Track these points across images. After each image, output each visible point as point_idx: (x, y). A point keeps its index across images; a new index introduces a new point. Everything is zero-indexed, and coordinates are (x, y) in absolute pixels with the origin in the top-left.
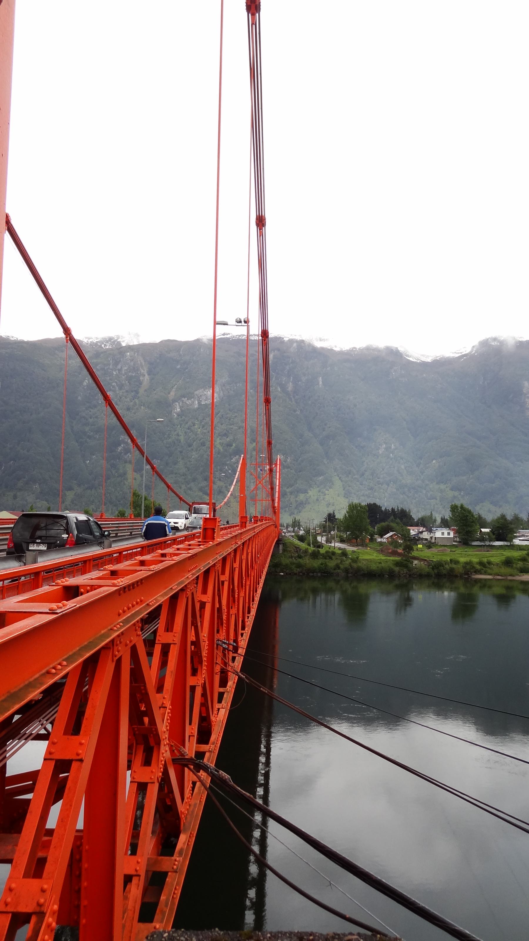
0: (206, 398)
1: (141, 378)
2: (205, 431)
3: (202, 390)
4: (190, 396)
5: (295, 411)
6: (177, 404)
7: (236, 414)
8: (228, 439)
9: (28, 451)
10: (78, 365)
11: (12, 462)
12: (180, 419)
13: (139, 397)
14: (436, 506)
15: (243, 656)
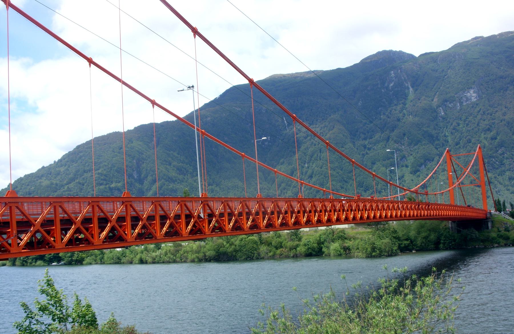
1: (406, 91)
7: (496, 109)
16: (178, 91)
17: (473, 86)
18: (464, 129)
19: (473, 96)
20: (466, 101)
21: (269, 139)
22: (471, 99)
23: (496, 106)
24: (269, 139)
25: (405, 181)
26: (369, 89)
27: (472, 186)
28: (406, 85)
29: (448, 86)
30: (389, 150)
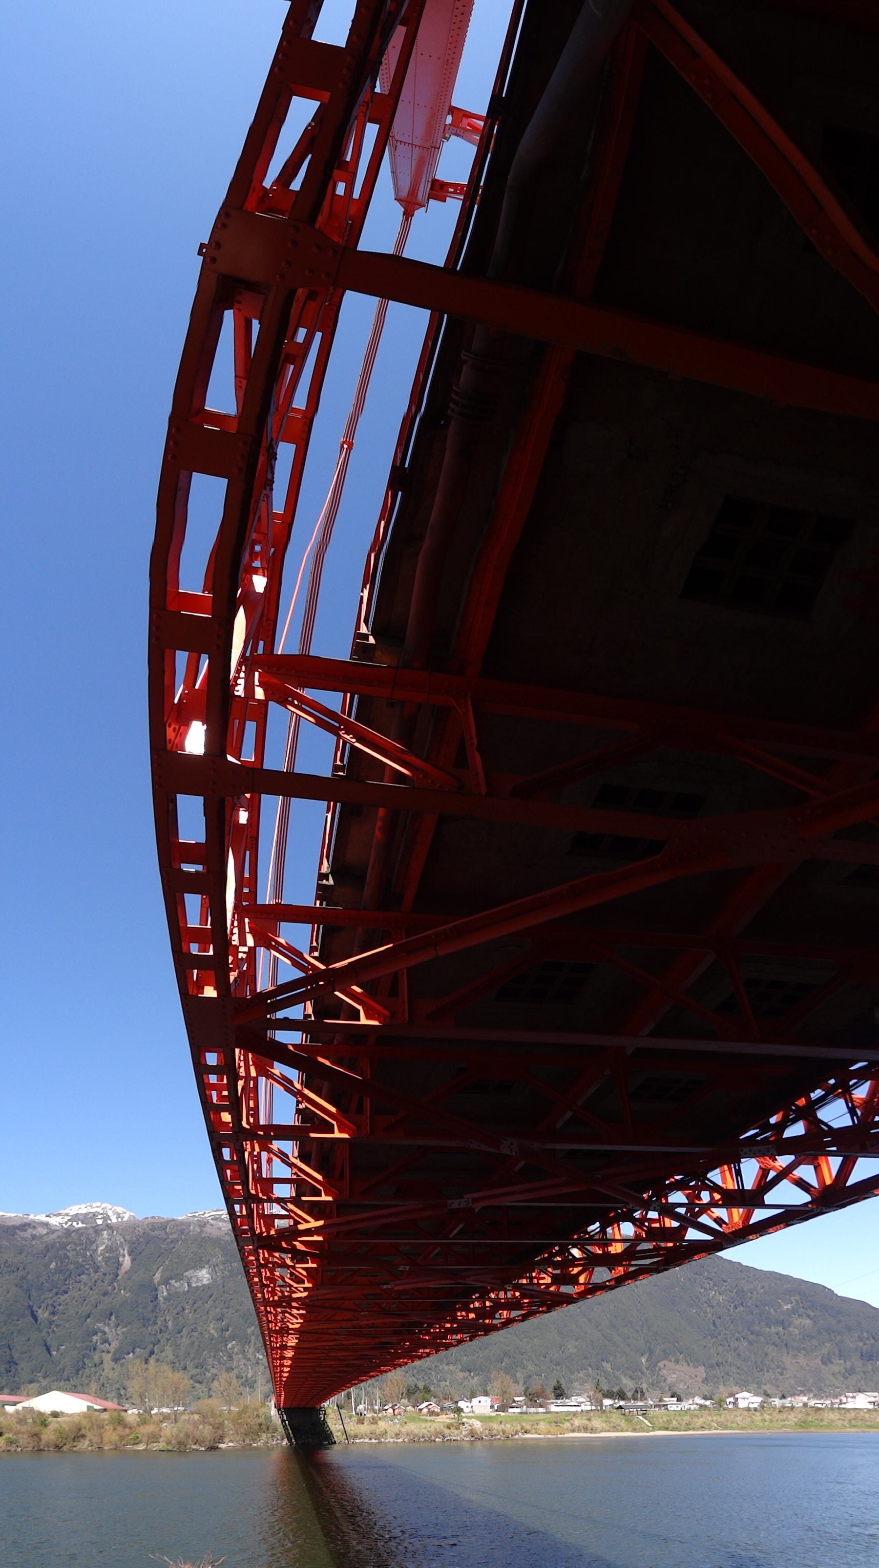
0: (198, 1280)
1: (121, 1259)
2: (196, 1316)
3: (193, 1271)
4: (179, 1277)
7: (232, 1297)
12: (168, 1303)
13: (118, 1281)
14: (446, 1388)
16: (426, 212)
17: (207, 1266)
18: (190, 1315)
19: (205, 1278)
20: (196, 1282)
22: (202, 1281)
23: (231, 1292)
25: (104, 1370)
26: (68, 1248)
27: (191, 1382)
28: (122, 1252)
29: (176, 1260)
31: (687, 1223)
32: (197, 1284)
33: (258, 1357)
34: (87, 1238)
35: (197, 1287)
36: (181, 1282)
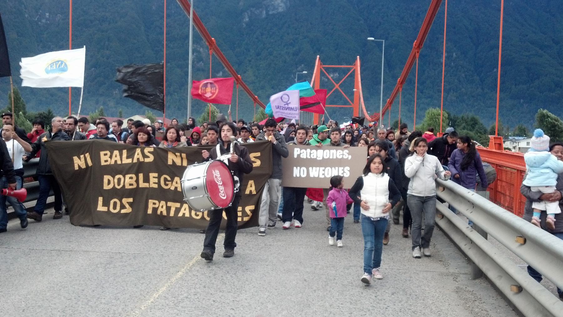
2: (272, 40)
5: (359, 20)
6: (246, 13)
8: (294, 49)
9: (107, 59)
10: (363, 285)
11: (93, 69)
15: (122, 162)
21: (48, 17)
22: (277, 9)
24: (48, 17)
30: (373, 39)
31: (376, 41)
32: (274, 12)
33: (323, 80)
34: (66, 131)
35: (273, 15)
36: (260, 9)
